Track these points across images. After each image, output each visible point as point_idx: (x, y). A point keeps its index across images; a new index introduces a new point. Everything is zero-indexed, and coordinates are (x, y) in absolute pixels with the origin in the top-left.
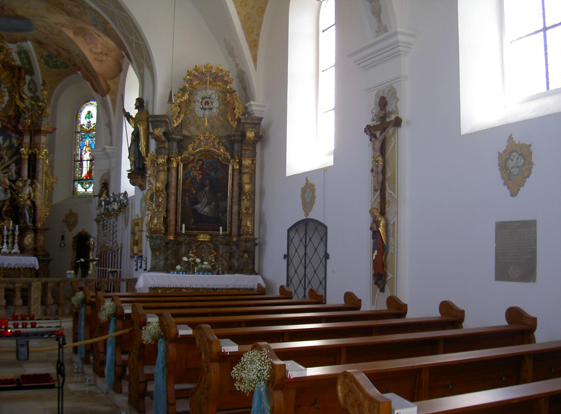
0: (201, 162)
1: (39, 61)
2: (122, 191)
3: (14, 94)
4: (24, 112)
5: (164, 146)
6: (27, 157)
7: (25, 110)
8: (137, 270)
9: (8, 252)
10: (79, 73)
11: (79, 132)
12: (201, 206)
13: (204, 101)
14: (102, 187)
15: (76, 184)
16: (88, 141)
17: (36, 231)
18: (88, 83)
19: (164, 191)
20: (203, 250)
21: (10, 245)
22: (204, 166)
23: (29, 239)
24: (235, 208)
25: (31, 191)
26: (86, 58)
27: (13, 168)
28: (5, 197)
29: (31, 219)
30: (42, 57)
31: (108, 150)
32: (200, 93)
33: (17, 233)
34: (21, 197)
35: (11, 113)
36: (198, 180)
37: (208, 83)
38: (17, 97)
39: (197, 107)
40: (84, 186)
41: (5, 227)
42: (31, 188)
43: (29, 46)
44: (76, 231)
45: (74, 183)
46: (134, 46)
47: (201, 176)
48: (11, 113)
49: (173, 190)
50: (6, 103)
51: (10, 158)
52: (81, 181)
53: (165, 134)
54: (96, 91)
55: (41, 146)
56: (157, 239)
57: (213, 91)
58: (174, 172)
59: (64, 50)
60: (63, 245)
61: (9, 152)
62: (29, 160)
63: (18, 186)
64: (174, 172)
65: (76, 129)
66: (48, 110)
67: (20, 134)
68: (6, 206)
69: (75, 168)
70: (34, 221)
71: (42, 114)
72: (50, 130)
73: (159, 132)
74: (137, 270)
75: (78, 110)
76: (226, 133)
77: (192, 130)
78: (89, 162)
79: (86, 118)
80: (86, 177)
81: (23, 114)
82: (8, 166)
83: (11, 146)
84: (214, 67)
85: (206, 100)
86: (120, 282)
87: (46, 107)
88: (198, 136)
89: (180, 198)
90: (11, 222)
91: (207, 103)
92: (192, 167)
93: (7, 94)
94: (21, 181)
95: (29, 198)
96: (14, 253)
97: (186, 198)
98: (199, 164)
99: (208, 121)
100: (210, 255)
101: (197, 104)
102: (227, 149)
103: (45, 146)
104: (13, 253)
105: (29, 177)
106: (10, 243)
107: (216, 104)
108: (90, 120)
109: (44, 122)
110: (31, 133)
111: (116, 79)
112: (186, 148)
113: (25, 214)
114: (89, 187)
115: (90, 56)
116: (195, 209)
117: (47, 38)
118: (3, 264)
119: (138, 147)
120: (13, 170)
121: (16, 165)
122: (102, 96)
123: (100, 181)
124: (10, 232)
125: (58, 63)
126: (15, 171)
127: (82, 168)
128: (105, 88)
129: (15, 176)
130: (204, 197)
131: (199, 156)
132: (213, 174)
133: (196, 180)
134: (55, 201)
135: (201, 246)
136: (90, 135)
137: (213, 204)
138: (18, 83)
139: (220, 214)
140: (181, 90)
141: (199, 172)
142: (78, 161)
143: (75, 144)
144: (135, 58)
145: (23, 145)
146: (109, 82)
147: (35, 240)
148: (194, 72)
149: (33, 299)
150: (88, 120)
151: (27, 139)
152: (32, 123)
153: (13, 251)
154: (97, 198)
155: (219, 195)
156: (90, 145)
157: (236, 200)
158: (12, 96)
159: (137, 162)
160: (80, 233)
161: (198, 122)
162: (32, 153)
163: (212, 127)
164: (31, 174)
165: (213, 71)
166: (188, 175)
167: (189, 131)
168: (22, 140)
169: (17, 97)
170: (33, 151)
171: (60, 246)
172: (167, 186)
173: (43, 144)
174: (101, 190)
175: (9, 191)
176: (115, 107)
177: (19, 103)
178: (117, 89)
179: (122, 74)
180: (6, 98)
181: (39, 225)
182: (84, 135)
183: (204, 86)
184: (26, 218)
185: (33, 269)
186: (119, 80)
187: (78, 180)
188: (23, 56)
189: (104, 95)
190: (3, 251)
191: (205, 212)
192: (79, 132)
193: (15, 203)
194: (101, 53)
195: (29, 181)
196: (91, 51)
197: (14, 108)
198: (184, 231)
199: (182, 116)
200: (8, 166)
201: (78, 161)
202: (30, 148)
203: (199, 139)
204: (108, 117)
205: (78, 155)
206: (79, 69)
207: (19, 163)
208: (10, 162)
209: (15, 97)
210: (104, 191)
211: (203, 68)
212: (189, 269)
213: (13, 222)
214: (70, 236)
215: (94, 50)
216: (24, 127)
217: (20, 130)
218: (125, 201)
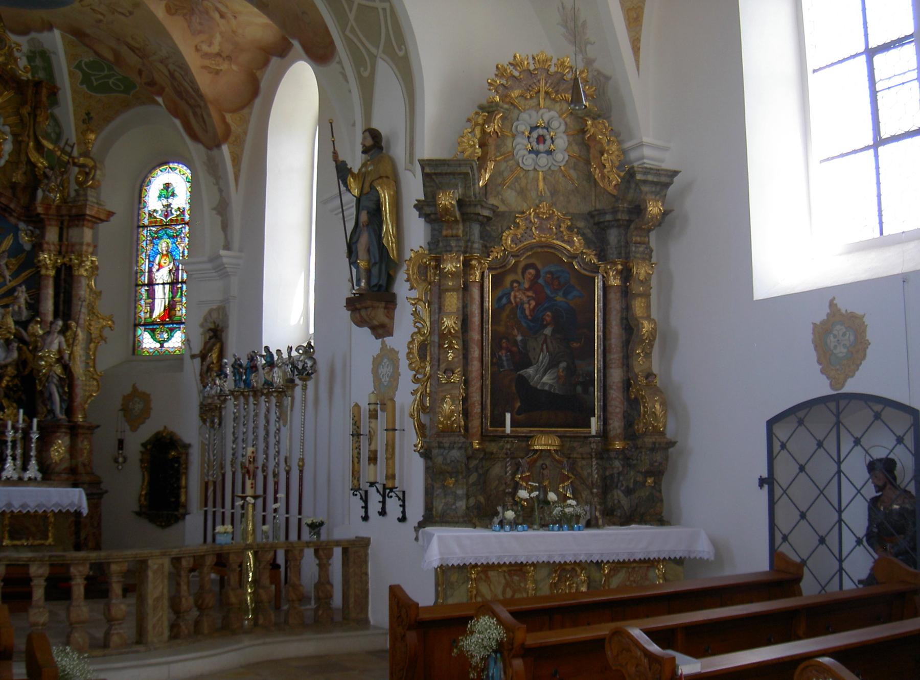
0: (532, 271)
1: (71, 75)
2: (264, 345)
3: (26, 139)
4: (46, 176)
5: (454, 232)
6: (52, 273)
7: (50, 173)
8: (366, 518)
9: (15, 477)
10: (160, 100)
11: (144, 227)
12: (537, 371)
13: (535, 135)
14: (210, 338)
15: (139, 332)
16: (164, 245)
17: (74, 430)
18: (177, 122)
19: (460, 335)
20: (546, 472)
21: (19, 462)
22: (541, 281)
23: (59, 450)
24: (616, 375)
25: (65, 346)
26: (184, 68)
27: (22, 296)
28: (6, 358)
29: (64, 406)
30: (79, 67)
31: (225, 260)
32: (524, 116)
33: (35, 436)
34: (41, 358)
35: (18, 177)
36: (527, 312)
37: (542, 95)
38: (31, 144)
39: (521, 146)
40: (158, 337)
41: (10, 424)
42: (63, 339)
43: (55, 41)
44: (147, 431)
45: (135, 331)
46: (351, 16)
47: (533, 303)
48: (18, 177)
49: (475, 336)
50: (6, 157)
51: (15, 275)
52: (152, 327)
53: (460, 203)
54: (194, 137)
55: (85, 248)
56: (451, 448)
57: (553, 113)
58: (476, 292)
59: (132, 49)
60: (121, 460)
61: (13, 261)
62: (57, 278)
63: (34, 335)
64: (476, 292)
65: (139, 220)
66: (98, 172)
67: (37, 222)
68: (7, 378)
69: (137, 300)
70: (69, 411)
71: (86, 181)
72: (102, 217)
73: (447, 200)
74: (366, 518)
75: (144, 181)
76: (585, 208)
77: (510, 199)
78: (167, 287)
79: (160, 197)
80: (162, 318)
81: (46, 181)
82: (12, 291)
83: (16, 249)
84: (554, 61)
85: (541, 131)
86: (332, 549)
87: (95, 167)
88: (523, 213)
89: (488, 351)
90: (21, 411)
91: (541, 139)
92: (512, 282)
93: (9, 137)
94: (40, 323)
95: (60, 360)
96: (30, 479)
97: (503, 353)
98: (527, 276)
99: (544, 179)
100: (563, 482)
101: (519, 140)
102: (588, 243)
103: (91, 249)
104: (26, 479)
105: (56, 315)
106: (18, 457)
107: (562, 142)
108: (170, 200)
109: (90, 198)
110: (62, 223)
111: (245, 111)
112: (499, 240)
113: (51, 395)
114: (169, 339)
115: (193, 61)
116: (521, 377)
117: (100, 21)
118: (9, 505)
119: (379, 238)
120: (22, 301)
121: (28, 289)
122: (209, 148)
123: (202, 326)
124: (19, 435)
125: (111, 81)
126: (27, 302)
127: (154, 299)
128: (220, 130)
129: (25, 314)
130: (542, 350)
131: (528, 257)
132: (559, 298)
133: (523, 310)
134: (102, 367)
135: (540, 462)
136: (170, 232)
137: (563, 365)
138: (34, 115)
139: (579, 389)
140: (482, 108)
141: (530, 294)
142: (144, 285)
143: (138, 250)
144: (350, 44)
145: (45, 246)
146: (228, 117)
147: (72, 450)
148: (510, 69)
149: (150, 602)
150: (165, 202)
151: (52, 235)
152: (64, 200)
153: (28, 474)
154: (198, 361)
155: (575, 345)
156: (169, 253)
157: (615, 356)
158: (20, 143)
159: (375, 271)
160: (158, 433)
161: (523, 182)
162: (64, 264)
163: (554, 192)
164: (61, 308)
165: (553, 69)
166: (504, 301)
167: (503, 201)
168: (42, 235)
169: (31, 144)
170: (66, 260)
171: (116, 461)
172: (465, 322)
173: (88, 245)
174: (206, 344)
175: (16, 345)
176: (239, 171)
177: (34, 157)
178: (245, 133)
179: (258, 101)
180: (8, 147)
181: (80, 418)
182: (156, 232)
183: (533, 103)
184: (53, 403)
185: (78, 514)
186: (250, 113)
187: (143, 325)
188: (38, 62)
189: (213, 144)
190: (5, 475)
191: (544, 384)
192: (144, 227)
193: (27, 372)
194: (219, 55)
195: (60, 323)
196: (197, 49)
197: (23, 167)
198: (508, 429)
199: (491, 165)
200: (12, 291)
201: (144, 285)
202: (60, 253)
203: (527, 219)
204: (221, 191)
205: (143, 272)
206: (160, 93)
207: (34, 284)
208: (13, 284)
209: (28, 145)
210: (214, 345)
211: (531, 61)
212: (533, 516)
213: (24, 413)
214: (136, 440)
215: (205, 48)
216: (48, 207)
217: (39, 214)
218: (309, 363)
